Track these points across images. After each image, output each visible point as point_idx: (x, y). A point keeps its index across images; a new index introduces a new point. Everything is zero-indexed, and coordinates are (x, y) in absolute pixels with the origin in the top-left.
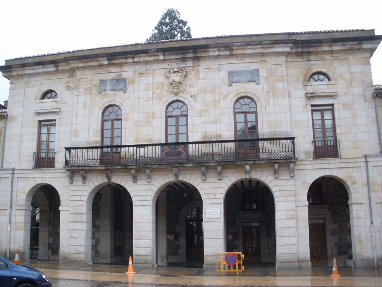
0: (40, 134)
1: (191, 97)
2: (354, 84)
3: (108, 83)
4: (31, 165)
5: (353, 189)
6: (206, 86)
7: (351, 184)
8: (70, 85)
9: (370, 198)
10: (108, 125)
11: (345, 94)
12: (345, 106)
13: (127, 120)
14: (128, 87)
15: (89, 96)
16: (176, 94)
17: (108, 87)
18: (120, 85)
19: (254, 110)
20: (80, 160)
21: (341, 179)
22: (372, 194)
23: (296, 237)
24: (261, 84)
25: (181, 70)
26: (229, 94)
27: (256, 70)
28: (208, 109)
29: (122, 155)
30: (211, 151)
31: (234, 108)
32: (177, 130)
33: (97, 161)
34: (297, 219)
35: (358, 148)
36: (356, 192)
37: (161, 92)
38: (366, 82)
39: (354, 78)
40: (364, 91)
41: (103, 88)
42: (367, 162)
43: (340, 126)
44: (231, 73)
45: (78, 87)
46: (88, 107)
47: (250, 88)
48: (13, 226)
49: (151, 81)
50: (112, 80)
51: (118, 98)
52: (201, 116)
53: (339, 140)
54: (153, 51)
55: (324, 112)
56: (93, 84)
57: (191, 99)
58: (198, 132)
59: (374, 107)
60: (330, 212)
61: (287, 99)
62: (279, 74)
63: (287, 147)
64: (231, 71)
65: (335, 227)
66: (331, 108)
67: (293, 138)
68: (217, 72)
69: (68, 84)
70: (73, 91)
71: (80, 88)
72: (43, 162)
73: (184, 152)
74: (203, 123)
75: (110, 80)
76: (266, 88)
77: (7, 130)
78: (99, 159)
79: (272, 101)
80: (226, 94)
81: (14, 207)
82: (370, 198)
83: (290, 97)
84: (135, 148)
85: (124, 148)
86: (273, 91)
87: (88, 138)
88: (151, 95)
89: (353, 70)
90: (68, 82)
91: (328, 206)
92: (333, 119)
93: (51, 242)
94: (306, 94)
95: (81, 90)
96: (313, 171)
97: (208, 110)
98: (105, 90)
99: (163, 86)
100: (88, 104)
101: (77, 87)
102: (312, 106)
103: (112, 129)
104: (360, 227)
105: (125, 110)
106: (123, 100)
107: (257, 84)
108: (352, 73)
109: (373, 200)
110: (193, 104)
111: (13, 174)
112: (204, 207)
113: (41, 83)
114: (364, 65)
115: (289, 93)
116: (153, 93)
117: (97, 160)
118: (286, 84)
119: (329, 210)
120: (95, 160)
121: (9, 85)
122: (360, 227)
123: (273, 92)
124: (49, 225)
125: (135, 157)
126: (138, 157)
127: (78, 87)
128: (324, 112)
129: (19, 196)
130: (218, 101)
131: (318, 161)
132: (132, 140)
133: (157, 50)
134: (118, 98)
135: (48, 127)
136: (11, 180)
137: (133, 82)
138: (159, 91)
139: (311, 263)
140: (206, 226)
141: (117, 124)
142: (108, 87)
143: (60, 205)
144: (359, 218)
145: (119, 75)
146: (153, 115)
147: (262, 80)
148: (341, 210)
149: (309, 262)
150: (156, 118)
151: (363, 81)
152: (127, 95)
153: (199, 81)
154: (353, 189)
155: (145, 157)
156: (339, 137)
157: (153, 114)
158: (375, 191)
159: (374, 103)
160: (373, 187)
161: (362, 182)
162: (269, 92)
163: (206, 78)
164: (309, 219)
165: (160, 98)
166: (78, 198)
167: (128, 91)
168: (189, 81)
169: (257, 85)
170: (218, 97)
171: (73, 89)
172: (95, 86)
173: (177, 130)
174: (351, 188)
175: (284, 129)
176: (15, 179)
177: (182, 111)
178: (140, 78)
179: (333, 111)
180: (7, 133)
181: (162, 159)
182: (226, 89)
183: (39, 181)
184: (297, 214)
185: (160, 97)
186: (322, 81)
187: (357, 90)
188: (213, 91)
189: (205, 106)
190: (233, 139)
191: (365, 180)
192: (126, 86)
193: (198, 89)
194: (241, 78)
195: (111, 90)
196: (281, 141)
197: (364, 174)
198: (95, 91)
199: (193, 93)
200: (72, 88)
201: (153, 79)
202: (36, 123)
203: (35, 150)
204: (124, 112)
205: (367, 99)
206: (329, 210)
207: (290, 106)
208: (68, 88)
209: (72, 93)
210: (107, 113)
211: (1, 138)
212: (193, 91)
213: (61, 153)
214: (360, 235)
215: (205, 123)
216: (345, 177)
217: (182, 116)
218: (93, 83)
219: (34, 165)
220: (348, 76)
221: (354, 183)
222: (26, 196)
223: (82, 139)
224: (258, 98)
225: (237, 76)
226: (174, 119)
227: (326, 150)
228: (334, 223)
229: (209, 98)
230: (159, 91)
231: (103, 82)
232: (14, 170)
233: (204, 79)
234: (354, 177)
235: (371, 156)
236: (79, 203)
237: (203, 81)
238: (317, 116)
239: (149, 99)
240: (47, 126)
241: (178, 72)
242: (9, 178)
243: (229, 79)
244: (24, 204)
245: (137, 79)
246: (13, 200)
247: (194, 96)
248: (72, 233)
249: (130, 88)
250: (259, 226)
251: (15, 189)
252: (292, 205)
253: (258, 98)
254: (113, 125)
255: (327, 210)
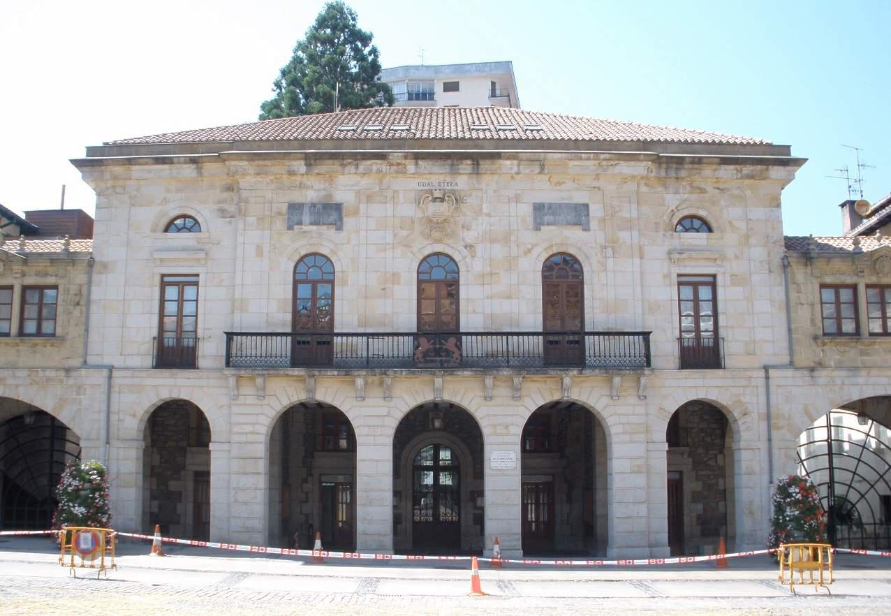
0: (162, 301)
1: (466, 248)
2: (753, 241)
3: (306, 210)
4: (149, 361)
5: (743, 423)
6: (492, 228)
7: (741, 415)
8: (225, 206)
9: (770, 440)
10: (172, 292)
11: (737, 257)
12: (736, 280)
13: (344, 283)
14: (345, 219)
15: (267, 233)
16: (438, 241)
17: (306, 218)
18: (329, 215)
19: (330, 277)
20: (261, 357)
21: (723, 406)
22: (775, 434)
23: (646, 505)
24: (591, 232)
25: (448, 197)
26: (534, 246)
27: (584, 205)
28: (497, 271)
29: (335, 350)
30: (505, 349)
31: (418, 273)
32: (180, 308)
33: (286, 360)
34: (648, 473)
35: (754, 354)
36: (747, 429)
37: (408, 236)
38: (773, 237)
39: (752, 229)
40: (769, 255)
41: (295, 218)
42: (767, 378)
43: (724, 313)
44: (539, 208)
45: (245, 212)
46: (266, 254)
47: (571, 239)
48: (114, 480)
49: (390, 213)
50: (314, 205)
51: (324, 240)
52: (483, 285)
53: (723, 339)
54: (398, 156)
55: (699, 287)
56: (274, 210)
57: (465, 252)
58: (477, 313)
59: (784, 283)
60: (691, 460)
61: (637, 261)
62: (626, 214)
63: (632, 347)
64: (540, 204)
65: (698, 486)
66: (712, 283)
67: (649, 333)
68: (513, 205)
69: (222, 205)
70: (232, 219)
71: (248, 216)
72: (175, 354)
73: (455, 349)
74: (488, 298)
75: (310, 205)
76: (601, 239)
77: (94, 289)
78: (289, 354)
79: (610, 262)
80: (530, 246)
81: (113, 442)
82: (770, 440)
83: (641, 257)
84: (365, 338)
85: (339, 338)
86: (611, 246)
87: (267, 315)
88: (390, 239)
89: (752, 216)
90: (220, 202)
91: (688, 448)
92: (714, 299)
93: (156, 510)
94: (670, 253)
95: (251, 220)
96: (682, 389)
97: (496, 273)
98: (300, 223)
99: (413, 222)
100: (266, 249)
101: (242, 213)
102: (679, 275)
103: (181, 301)
104: (751, 488)
105: (341, 264)
106: (336, 245)
107: (585, 230)
108: (750, 220)
109: (775, 444)
110: (468, 260)
111: (110, 377)
112: (487, 448)
113: (165, 198)
114: (770, 207)
115: (641, 248)
116: (395, 235)
117: (286, 357)
118: (635, 234)
119: (689, 457)
120: (251, 357)
121: (95, 197)
122: (751, 488)
123: (613, 249)
124: (151, 476)
125: (365, 354)
126: (370, 355)
127: (245, 212)
128: (699, 287)
129: (122, 421)
130: (514, 257)
131: (686, 372)
132: (356, 322)
133: (405, 156)
134: (324, 240)
135: (179, 289)
136: (106, 391)
137: (356, 212)
138: (404, 233)
139: (669, 548)
140: (490, 483)
141: (189, 292)
142: (306, 218)
143: (210, 441)
144: (750, 474)
145: (326, 196)
146: (395, 278)
147: (594, 224)
148: (709, 456)
149: (663, 546)
150: (399, 284)
151: (767, 237)
152: (344, 234)
153: (480, 218)
154: (743, 423)
155: (383, 355)
156: (722, 333)
157: (394, 274)
158: (778, 428)
159: (783, 275)
160: (776, 421)
161: (758, 412)
162: (606, 248)
163: (492, 214)
164: (668, 472)
165: (407, 246)
166: (249, 428)
167: (344, 228)
168: (463, 218)
169: (585, 233)
170: (515, 251)
171: (232, 217)
172: (280, 214)
173: (180, 308)
174: (740, 422)
175: (631, 319)
176: (115, 389)
177: (323, 273)
178: (369, 205)
179: (713, 285)
180: (94, 296)
181: (416, 360)
182: (529, 236)
183: (166, 395)
184: (648, 465)
185: (407, 245)
186: (697, 231)
187: (758, 253)
188: (506, 239)
189: (491, 266)
190: (541, 330)
191: (763, 410)
192: (341, 219)
193: (478, 234)
194: (557, 217)
195: (311, 224)
196: (622, 337)
197: (763, 399)
198: (280, 224)
199: (469, 241)
200: (229, 215)
201: (394, 209)
202: (157, 280)
203: (155, 333)
204: (337, 267)
205: (772, 270)
206: (689, 457)
207: (642, 273)
208: (223, 213)
209: (230, 223)
210: (302, 268)
211: (82, 305)
212: (470, 237)
213: (210, 340)
214: (751, 502)
215: (491, 297)
216: (730, 403)
217: (323, 281)
218: (275, 207)
219: (154, 363)
220: (742, 226)
221: (745, 414)
222: (138, 422)
223: (251, 319)
224: (586, 256)
225: (550, 214)
226: (309, 286)
227: (702, 355)
228: (697, 480)
229: (498, 251)
230: (404, 233)
231: (295, 208)
232: (111, 369)
233: (489, 215)
234: (746, 403)
235: (774, 367)
236: (251, 438)
237: (487, 219)
238: (829, 295)
239: (388, 246)
240: (178, 285)
241: (442, 200)
242: (102, 387)
243: (535, 218)
244: (135, 437)
245: (363, 207)
246: (112, 430)
247: (471, 246)
248: (236, 493)
249: (348, 222)
250: (551, 480)
251: (114, 407)
252: (639, 450)
253: (586, 256)
254: (181, 293)
255: (685, 456)
